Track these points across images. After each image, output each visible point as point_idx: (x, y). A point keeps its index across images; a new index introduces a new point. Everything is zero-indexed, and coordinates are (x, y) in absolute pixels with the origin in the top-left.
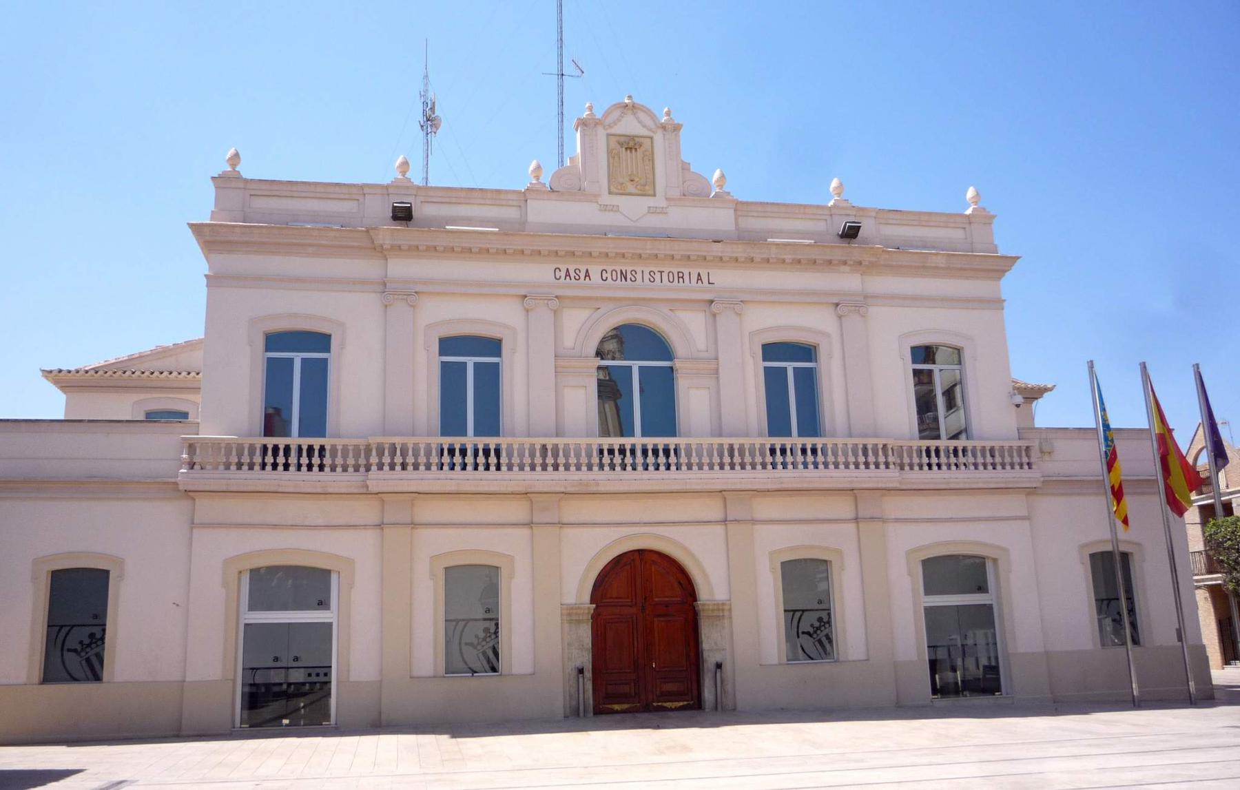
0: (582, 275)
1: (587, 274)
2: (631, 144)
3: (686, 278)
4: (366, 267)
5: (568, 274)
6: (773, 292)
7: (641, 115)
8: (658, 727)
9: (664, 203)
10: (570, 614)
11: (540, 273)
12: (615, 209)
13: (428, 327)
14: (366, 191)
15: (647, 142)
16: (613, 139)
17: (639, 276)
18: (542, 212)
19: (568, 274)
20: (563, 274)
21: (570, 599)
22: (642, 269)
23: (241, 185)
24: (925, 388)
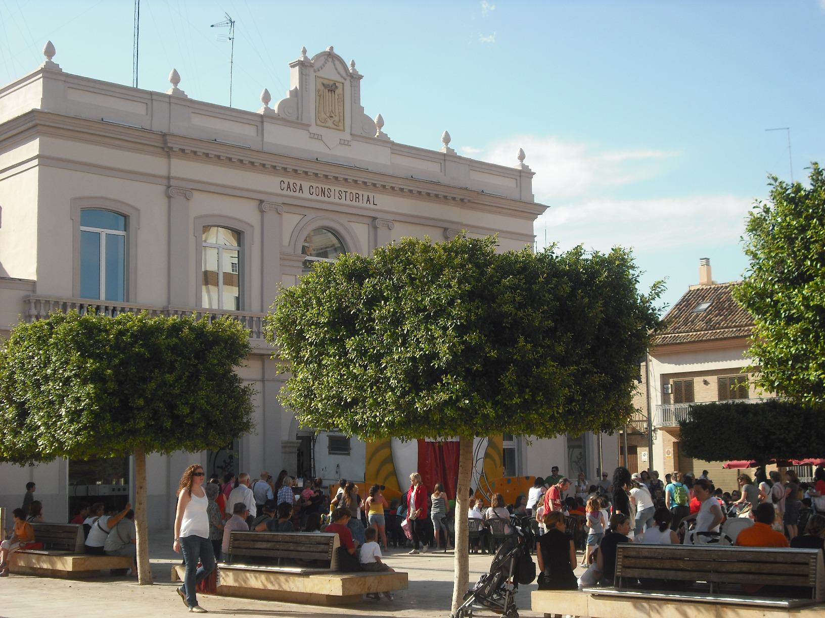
0: (298, 188)
1: (301, 189)
2: (332, 88)
3: (361, 198)
4: (155, 164)
5: (289, 187)
6: (128, 279)
7: (337, 62)
8: (311, 594)
9: (348, 138)
10: (286, 445)
11: (269, 184)
12: (318, 137)
13: (196, 218)
14: (154, 97)
15: (340, 86)
16: (320, 81)
17: (332, 194)
18: (280, 138)
19: (289, 187)
20: (285, 186)
21: (285, 438)
22: (306, 185)
23: (63, 78)
24: (577, 452)
